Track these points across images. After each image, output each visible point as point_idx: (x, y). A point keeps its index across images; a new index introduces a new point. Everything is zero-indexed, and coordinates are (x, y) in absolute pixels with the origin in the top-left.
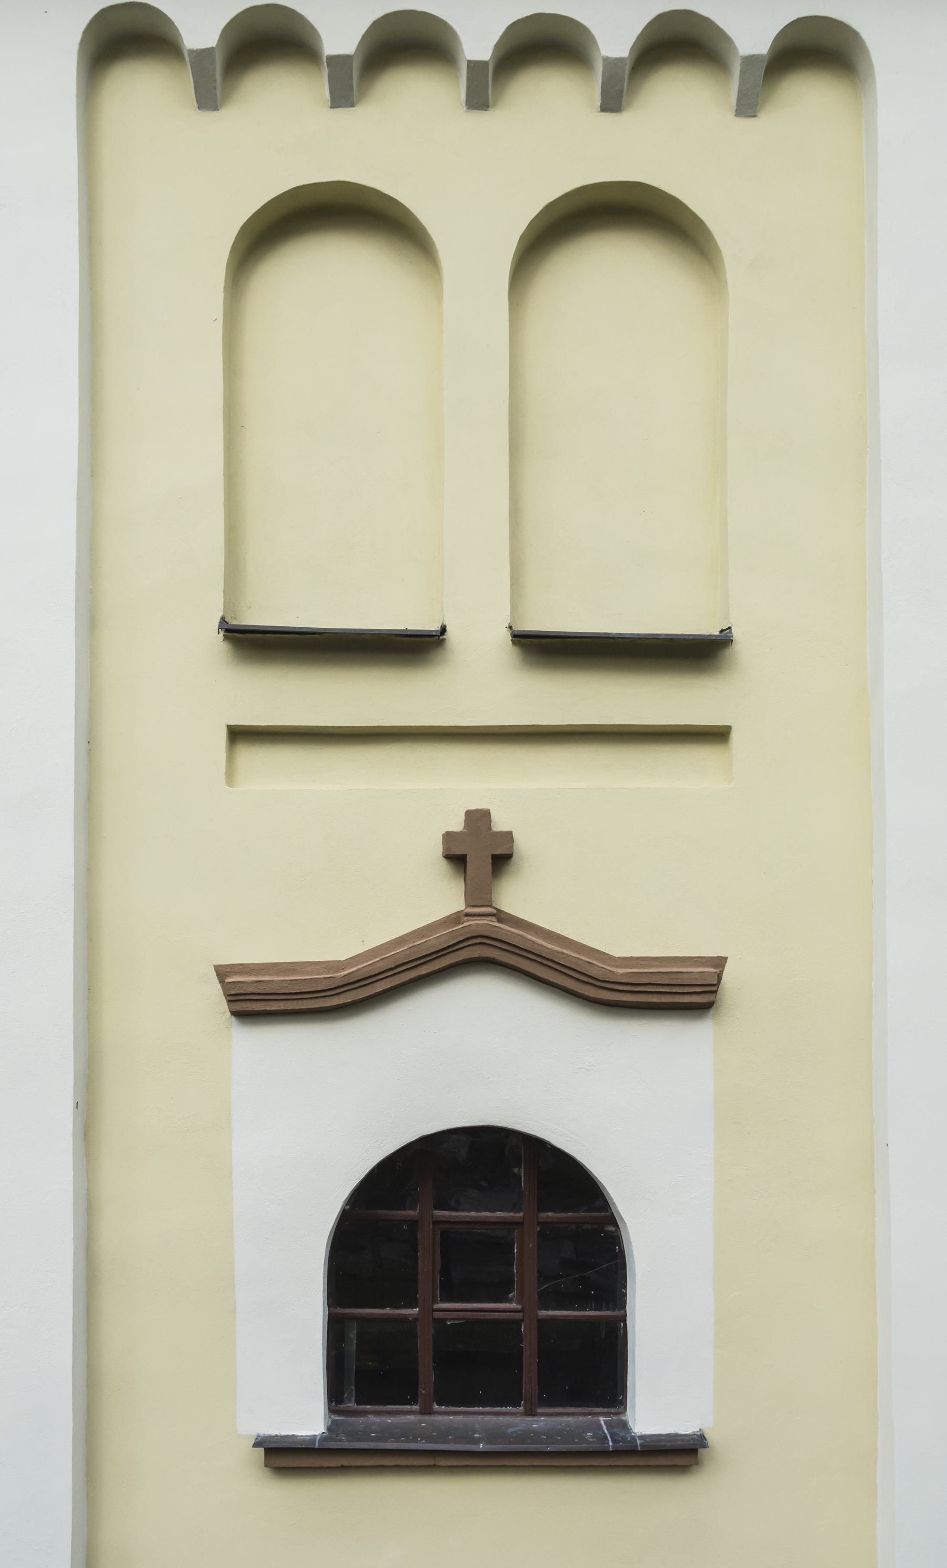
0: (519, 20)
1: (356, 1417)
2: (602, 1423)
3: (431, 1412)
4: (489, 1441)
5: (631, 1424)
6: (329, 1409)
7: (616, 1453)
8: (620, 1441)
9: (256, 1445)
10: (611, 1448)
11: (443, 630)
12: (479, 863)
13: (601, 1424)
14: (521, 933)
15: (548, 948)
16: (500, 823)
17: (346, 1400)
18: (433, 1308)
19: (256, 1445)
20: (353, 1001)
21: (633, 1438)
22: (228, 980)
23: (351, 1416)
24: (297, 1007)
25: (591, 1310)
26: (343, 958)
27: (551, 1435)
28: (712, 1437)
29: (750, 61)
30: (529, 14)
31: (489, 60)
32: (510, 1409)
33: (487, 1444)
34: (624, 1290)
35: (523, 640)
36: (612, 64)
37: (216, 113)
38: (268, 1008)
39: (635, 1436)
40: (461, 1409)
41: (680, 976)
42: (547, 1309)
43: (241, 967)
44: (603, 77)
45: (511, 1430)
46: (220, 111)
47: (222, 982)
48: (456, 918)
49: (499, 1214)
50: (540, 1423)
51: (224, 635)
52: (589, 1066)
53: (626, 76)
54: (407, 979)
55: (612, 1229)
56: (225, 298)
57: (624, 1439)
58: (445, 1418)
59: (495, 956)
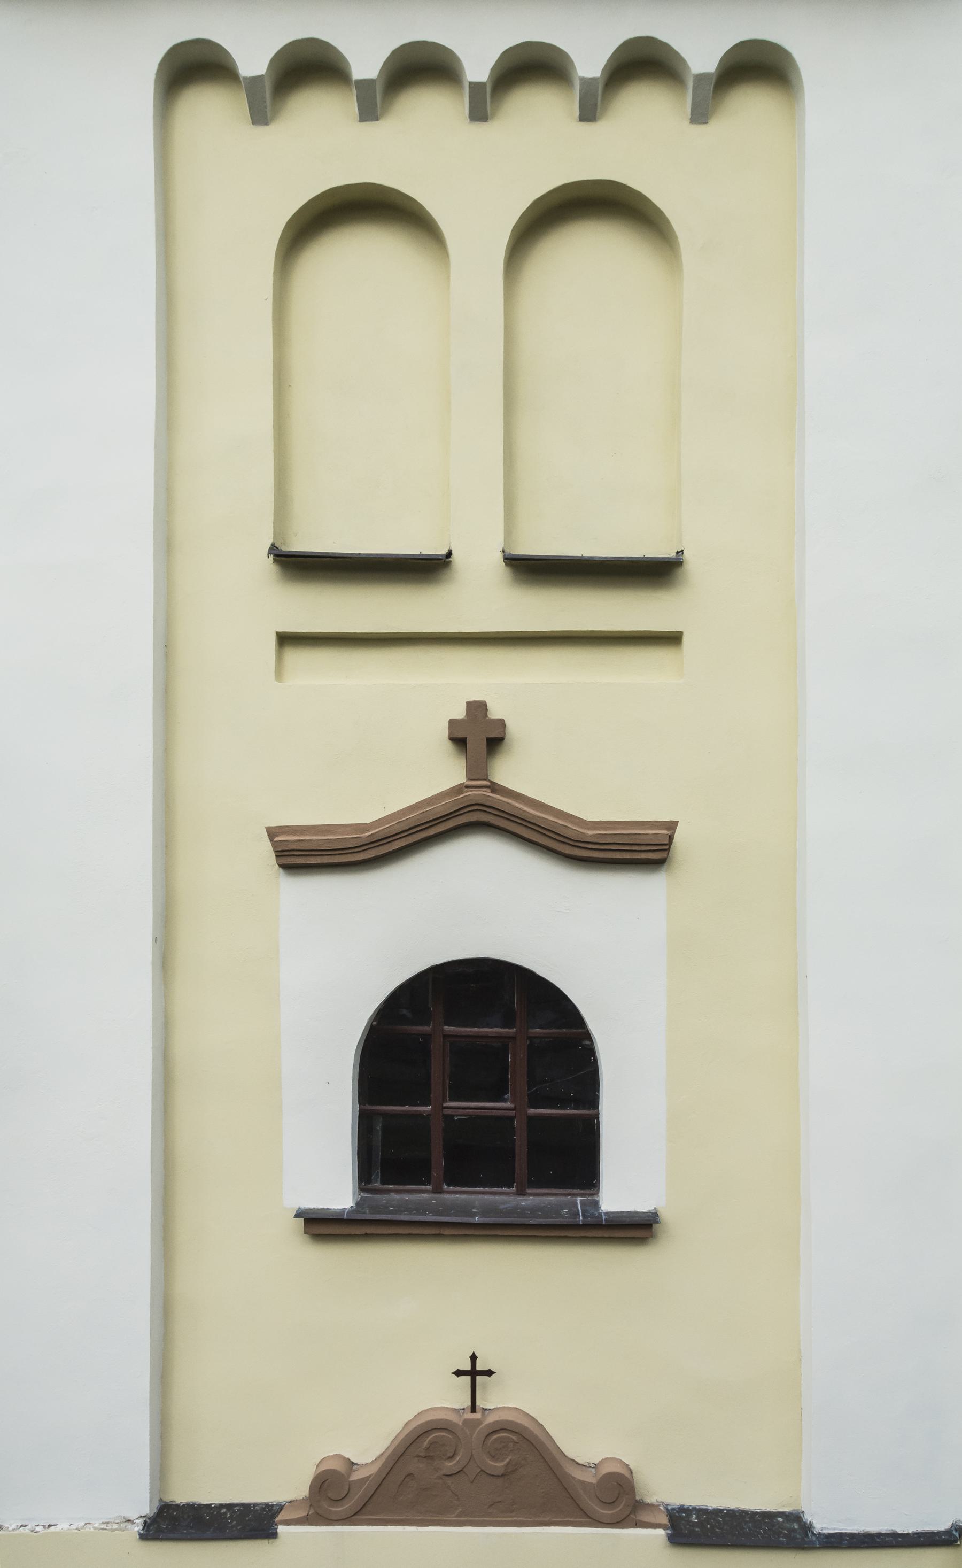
0: (511, 47)
1: (381, 1195)
2: (579, 1202)
3: (440, 1191)
4: (484, 1213)
5: (600, 1203)
6: (359, 1188)
7: (586, 1226)
8: (588, 1217)
9: (297, 1216)
10: (581, 1221)
11: (449, 554)
12: (477, 744)
13: (577, 1203)
14: (510, 801)
15: (531, 814)
16: (495, 712)
17: (373, 1181)
18: (442, 1105)
19: (297, 1216)
20: (375, 856)
21: (600, 1214)
22: (276, 839)
23: (377, 1194)
24: (325, 861)
25: (571, 1109)
26: (368, 820)
27: (534, 1211)
28: (664, 1215)
29: (700, 78)
30: (519, 43)
31: (487, 81)
32: (505, 1189)
33: (481, 1218)
34: (597, 1093)
35: (513, 562)
36: (587, 84)
37: (266, 127)
38: (308, 862)
39: (601, 1213)
40: (466, 1189)
41: (642, 837)
42: (535, 1108)
43: (287, 829)
44: (580, 94)
45: (502, 1207)
46: (270, 126)
47: (271, 840)
48: (459, 789)
49: (496, 1030)
50: (526, 1201)
51: (273, 559)
52: (566, 910)
53: (600, 92)
54: (419, 839)
55: (587, 1042)
56: (275, 281)
57: (593, 1215)
58: (452, 1196)
59: (489, 820)
